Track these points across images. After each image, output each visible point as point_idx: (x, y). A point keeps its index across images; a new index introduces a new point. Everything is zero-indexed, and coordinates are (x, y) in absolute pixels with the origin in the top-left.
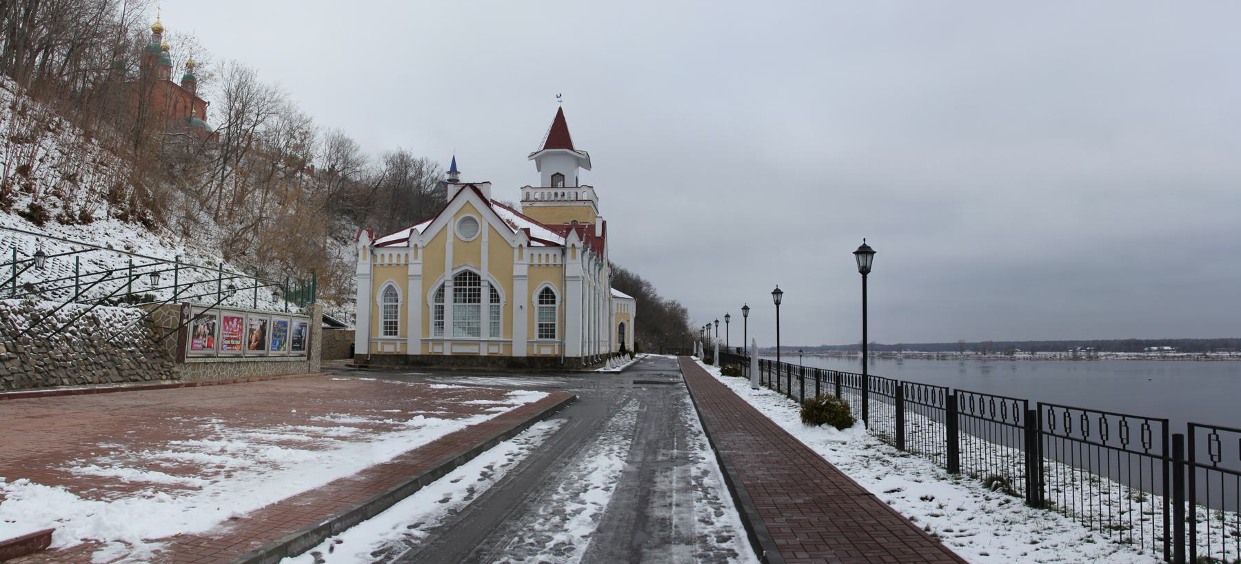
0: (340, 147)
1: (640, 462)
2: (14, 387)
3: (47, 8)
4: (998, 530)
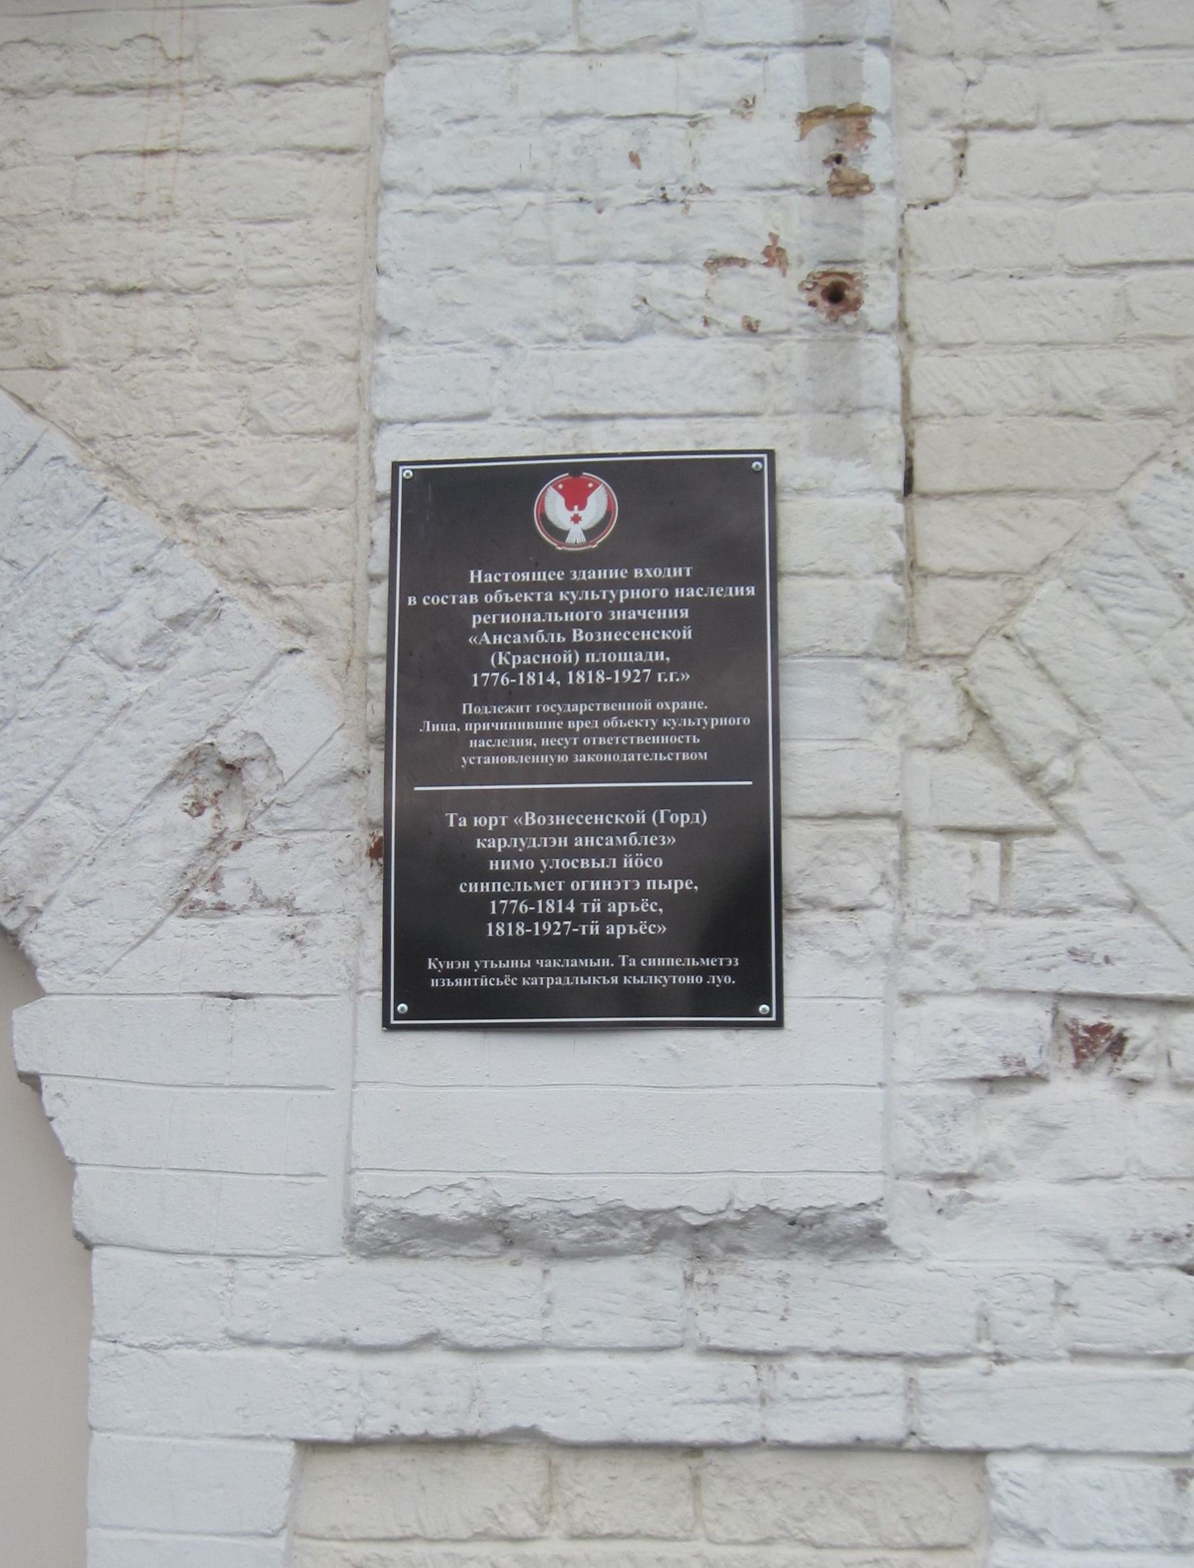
0: (925, 1004)
2: (399, 1008)
4: (838, 1331)
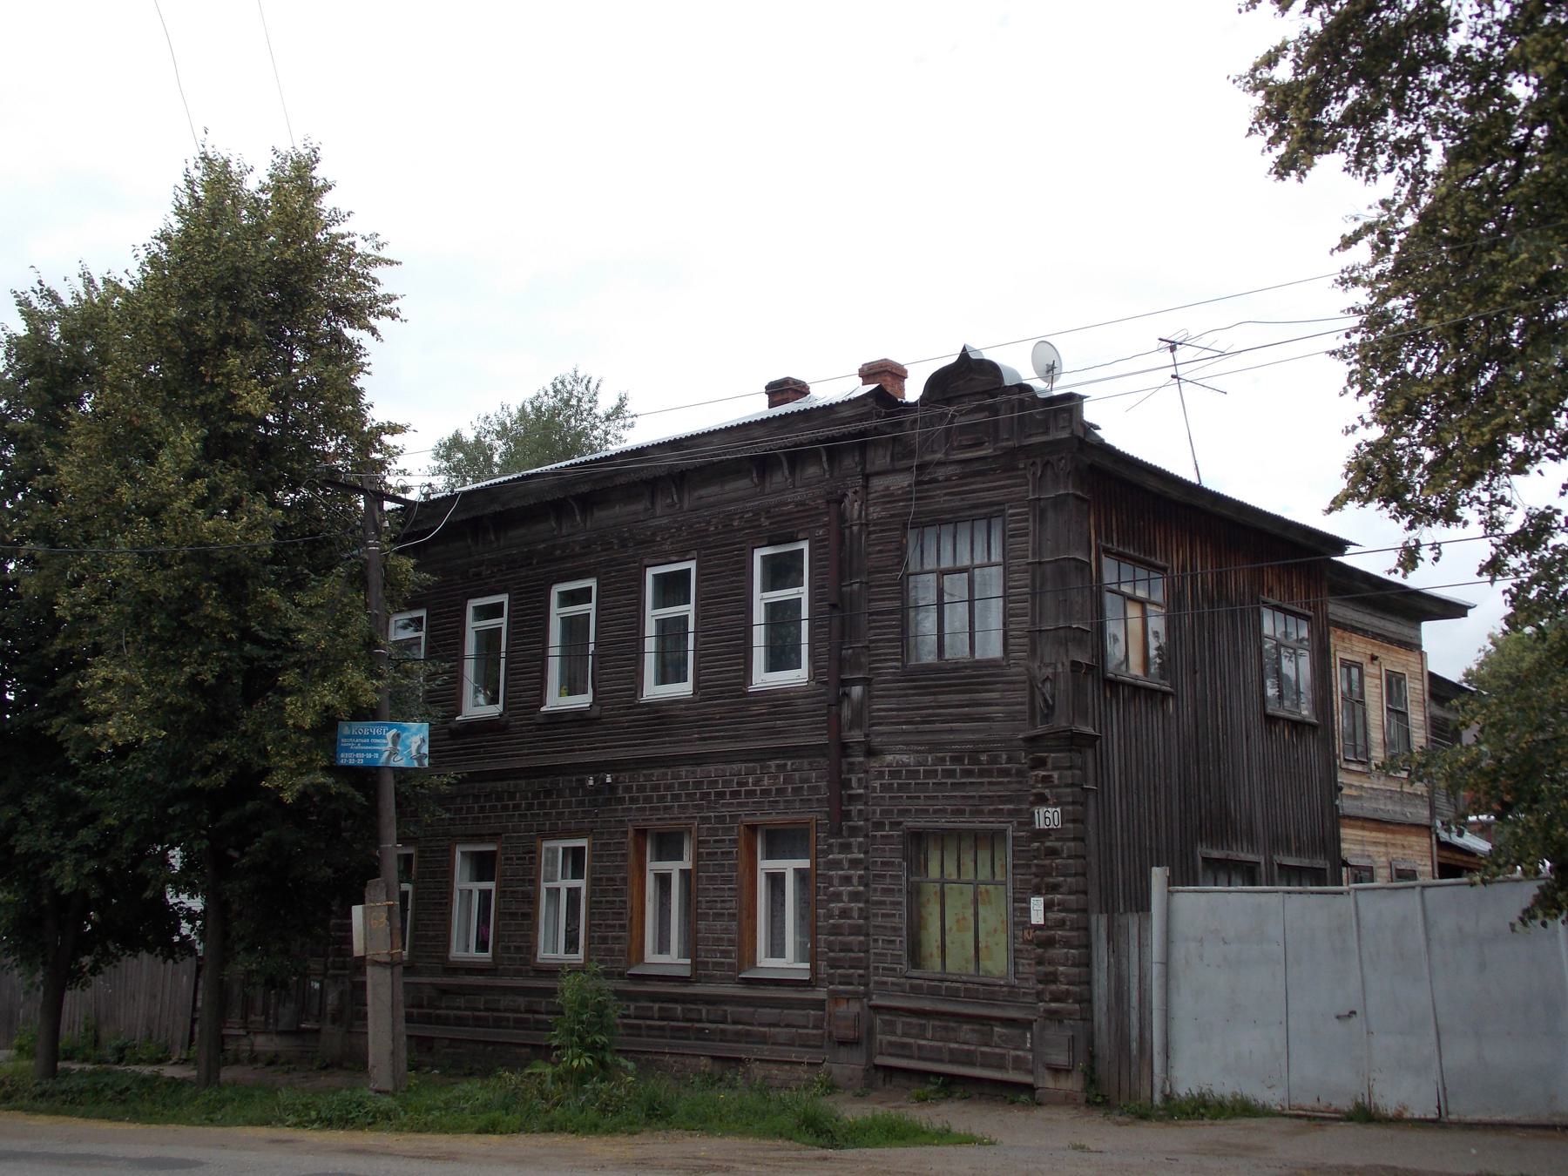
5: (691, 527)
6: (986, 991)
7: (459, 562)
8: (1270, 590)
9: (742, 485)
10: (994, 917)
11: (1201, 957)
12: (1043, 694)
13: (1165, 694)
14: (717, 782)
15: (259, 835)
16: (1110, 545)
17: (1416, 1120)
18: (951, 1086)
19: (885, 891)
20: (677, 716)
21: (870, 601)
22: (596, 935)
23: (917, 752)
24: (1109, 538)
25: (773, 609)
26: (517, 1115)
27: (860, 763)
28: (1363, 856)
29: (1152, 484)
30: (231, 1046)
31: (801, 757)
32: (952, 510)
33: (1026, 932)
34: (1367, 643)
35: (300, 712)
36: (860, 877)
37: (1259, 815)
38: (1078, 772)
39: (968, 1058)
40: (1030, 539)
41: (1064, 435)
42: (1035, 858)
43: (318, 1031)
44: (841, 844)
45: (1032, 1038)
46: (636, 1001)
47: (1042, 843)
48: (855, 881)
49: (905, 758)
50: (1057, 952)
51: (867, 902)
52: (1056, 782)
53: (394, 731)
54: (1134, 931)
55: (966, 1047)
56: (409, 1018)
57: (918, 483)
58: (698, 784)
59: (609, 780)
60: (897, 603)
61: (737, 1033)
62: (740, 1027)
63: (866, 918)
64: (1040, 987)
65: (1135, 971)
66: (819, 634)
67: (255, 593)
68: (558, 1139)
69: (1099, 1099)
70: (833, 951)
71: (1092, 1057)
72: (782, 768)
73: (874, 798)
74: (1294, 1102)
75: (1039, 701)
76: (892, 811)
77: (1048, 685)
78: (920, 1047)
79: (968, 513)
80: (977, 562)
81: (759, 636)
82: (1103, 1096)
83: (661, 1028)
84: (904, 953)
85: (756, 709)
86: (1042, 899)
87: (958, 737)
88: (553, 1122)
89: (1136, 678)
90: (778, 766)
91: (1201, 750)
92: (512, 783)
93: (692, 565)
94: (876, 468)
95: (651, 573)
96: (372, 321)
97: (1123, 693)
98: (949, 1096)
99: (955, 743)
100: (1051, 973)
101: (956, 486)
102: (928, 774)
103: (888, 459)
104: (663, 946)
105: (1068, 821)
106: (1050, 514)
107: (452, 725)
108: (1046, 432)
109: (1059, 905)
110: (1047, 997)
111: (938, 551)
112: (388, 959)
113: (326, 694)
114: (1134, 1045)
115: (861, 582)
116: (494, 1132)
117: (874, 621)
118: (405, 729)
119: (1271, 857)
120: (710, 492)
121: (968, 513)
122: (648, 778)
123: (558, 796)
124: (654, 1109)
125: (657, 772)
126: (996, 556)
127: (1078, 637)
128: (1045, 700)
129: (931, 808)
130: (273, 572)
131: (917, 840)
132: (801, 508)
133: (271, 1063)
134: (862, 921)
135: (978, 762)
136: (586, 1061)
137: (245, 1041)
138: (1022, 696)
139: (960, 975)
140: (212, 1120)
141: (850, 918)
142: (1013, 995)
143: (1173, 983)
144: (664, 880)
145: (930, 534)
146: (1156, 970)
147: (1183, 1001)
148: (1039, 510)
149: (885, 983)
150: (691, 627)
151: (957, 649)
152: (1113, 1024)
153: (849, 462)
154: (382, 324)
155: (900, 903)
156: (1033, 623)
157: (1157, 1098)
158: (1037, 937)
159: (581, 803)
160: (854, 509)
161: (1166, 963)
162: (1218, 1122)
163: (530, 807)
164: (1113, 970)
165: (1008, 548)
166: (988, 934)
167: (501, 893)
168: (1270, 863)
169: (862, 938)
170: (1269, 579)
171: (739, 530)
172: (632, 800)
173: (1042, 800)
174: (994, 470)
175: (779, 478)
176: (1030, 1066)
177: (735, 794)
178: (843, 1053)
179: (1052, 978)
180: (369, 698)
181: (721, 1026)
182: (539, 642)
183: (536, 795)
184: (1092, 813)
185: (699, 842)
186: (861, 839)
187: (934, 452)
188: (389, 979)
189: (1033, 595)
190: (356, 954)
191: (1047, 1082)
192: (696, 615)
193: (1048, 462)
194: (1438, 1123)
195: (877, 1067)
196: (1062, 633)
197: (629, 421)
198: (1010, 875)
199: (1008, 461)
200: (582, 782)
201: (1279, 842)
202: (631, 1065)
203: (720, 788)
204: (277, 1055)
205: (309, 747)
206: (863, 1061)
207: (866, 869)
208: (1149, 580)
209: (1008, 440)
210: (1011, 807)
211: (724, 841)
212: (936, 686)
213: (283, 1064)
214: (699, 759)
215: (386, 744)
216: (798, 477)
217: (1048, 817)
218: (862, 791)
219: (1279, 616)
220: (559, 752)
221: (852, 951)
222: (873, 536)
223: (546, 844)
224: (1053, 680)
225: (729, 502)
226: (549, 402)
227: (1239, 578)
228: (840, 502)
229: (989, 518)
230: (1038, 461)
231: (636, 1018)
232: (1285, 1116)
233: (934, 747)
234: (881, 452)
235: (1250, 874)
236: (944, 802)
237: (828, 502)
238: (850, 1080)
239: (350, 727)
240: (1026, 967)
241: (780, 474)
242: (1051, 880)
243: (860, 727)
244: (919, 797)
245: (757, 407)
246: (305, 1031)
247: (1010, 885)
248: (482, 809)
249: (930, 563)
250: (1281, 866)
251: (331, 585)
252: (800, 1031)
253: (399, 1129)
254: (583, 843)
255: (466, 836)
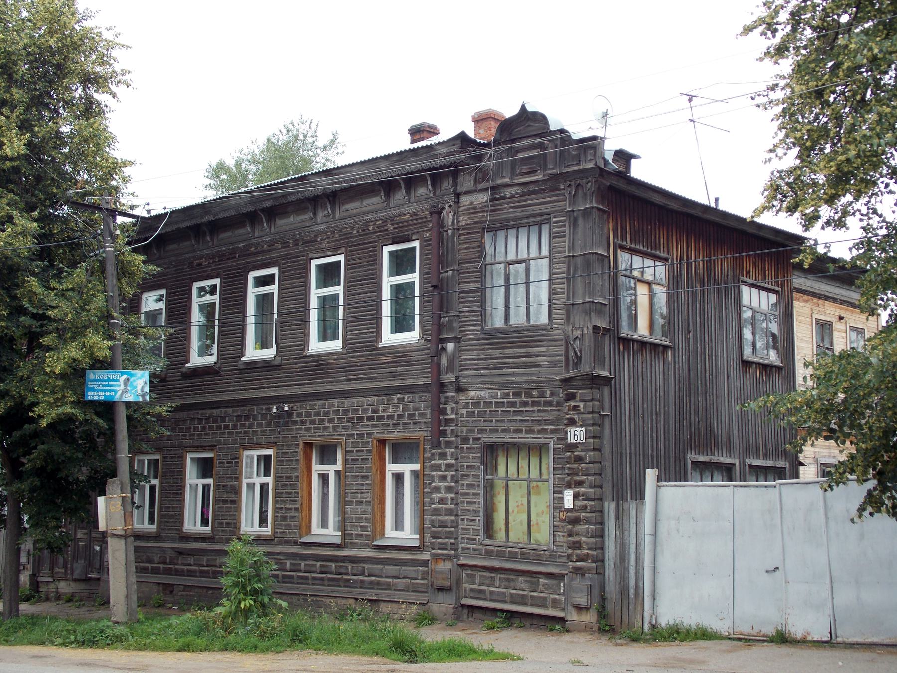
1: (312, 259)
3: (430, 528)
5: (341, 231)
6: (534, 555)
7: (187, 256)
8: (748, 273)
9: (375, 202)
10: (541, 504)
11: (678, 531)
12: (574, 349)
13: (665, 348)
14: (358, 410)
15: (35, 448)
16: (625, 243)
17: (814, 641)
18: (511, 619)
19: (470, 486)
20: (332, 364)
21: (460, 283)
22: (279, 515)
23: (492, 389)
24: (624, 238)
25: (324, 300)
26: (204, 639)
27: (453, 397)
28: (829, 457)
29: (657, 199)
30: (43, 589)
31: (413, 393)
32: (516, 219)
33: (561, 514)
34: (836, 307)
35: (56, 363)
36: (453, 476)
37: (735, 431)
38: (597, 403)
39: (522, 601)
40: (567, 239)
41: (590, 165)
42: (568, 463)
43: (99, 579)
44: (440, 454)
45: (564, 586)
46: (306, 561)
47: (572, 452)
48: (449, 479)
49: (483, 393)
50: (581, 528)
51: (457, 493)
52: (582, 410)
53: (125, 377)
54: (633, 513)
55: (521, 592)
56: (140, 570)
57: (492, 200)
58: (346, 412)
59: (286, 408)
60: (478, 285)
61: (371, 583)
62: (373, 578)
63: (457, 504)
64: (570, 551)
65: (633, 540)
66: (426, 306)
67: (24, 281)
68: (228, 655)
69: (607, 628)
70: (434, 527)
71: (603, 599)
72: (401, 400)
73: (462, 421)
74: (737, 630)
75: (571, 353)
76: (474, 430)
77: (578, 342)
78: (492, 593)
79: (526, 221)
80: (532, 255)
81: (387, 308)
82: (611, 626)
83: (322, 579)
84: (481, 528)
85: (384, 359)
86: (571, 491)
87: (519, 379)
88: (227, 644)
89: (643, 336)
90: (398, 399)
91: (692, 387)
92: (223, 410)
93: (341, 258)
94: (464, 189)
95: (314, 263)
96: (113, 88)
97: (634, 347)
98: (510, 626)
99: (516, 383)
100: (577, 542)
101: (518, 202)
102: (498, 404)
103: (473, 183)
104: (324, 524)
105: (590, 437)
106: (580, 222)
107: (183, 370)
108: (578, 164)
109: (583, 495)
110: (574, 558)
111: (506, 248)
112: (123, 533)
113: (73, 351)
114: (632, 591)
115: (454, 270)
116: (189, 651)
117: (463, 297)
118: (132, 375)
119: (744, 461)
120: (353, 206)
121: (526, 221)
122: (313, 407)
123: (254, 419)
124: (296, 636)
125: (319, 403)
126: (545, 251)
127: (598, 309)
128: (575, 353)
129: (500, 429)
130: (37, 266)
131: (491, 450)
132: (414, 218)
133: (69, 601)
134: (453, 507)
135: (531, 396)
136: (248, 602)
137: (52, 585)
138: (561, 350)
139: (518, 543)
140: (7, 641)
141: (446, 504)
142: (552, 557)
143: (659, 549)
144: (324, 477)
145: (501, 235)
146: (648, 540)
147: (666, 562)
148: (573, 219)
149: (468, 549)
150: (341, 302)
151: (518, 318)
152: (618, 577)
153: (447, 185)
154: (119, 90)
155: (479, 494)
156: (568, 299)
157: (646, 627)
158: (568, 517)
159: (269, 424)
160: (449, 218)
161: (655, 535)
162: (684, 643)
163: (235, 427)
164: (619, 540)
165: (552, 245)
166: (538, 515)
167: (217, 487)
168: (743, 464)
169: (453, 518)
170: (747, 265)
171: (372, 233)
172: (303, 422)
173: (572, 422)
174: (544, 190)
175: (400, 196)
176: (563, 606)
177: (370, 418)
178: (441, 596)
179: (577, 545)
180: (103, 353)
181: (361, 578)
182: (240, 312)
183: (239, 419)
184: (607, 431)
185: (347, 451)
186: (453, 450)
187: (503, 177)
188: (123, 547)
189: (568, 278)
190: (100, 530)
191: (573, 616)
192: (345, 293)
193: (579, 185)
194: (829, 644)
195: (463, 606)
196: (587, 305)
197: (340, 150)
198: (551, 475)
199: (554, 183)
200: (269, 410)
201: (750, 449)
202: (284, 604)
203: (360, 414)
204: (73, 595)
205: (62, 388)
206: (454, 602)
207: (457, 470)
208: (655, 266)
209: (552, 169)
210: (553, 427)
211: (362, 451)
212: (503, 343)
213: (76, 601)
214: (346, 394)
215: (120, 386)
216: (412, 195)
217: (576, 434)
218: (453, 417)
219: (755, 291)
220: (254, 389)
221: (446, 527)
222: (463, 237)
223: (247, 453)
224: (581, 338)
225: (366, 213)
226: (283, 138)
227: (723, 264)
228: (439, 213)
229: (540, 224)
230: (573, 183)
231: (305, 572)
232: (730, 639)
233: (502, 386)
234: (467, 178)
235: (727, 472)
236: (509, 424)
237: (431, 213)
238: (445, 615)
239: (94, 374)
240: (562, 538)
241: (400, 193)
242: (578, 478)
243: (453, 372)
244: (491, 421)
245: (404, 143)
246: (90, 579)
247: (551, 481)
248: (204, 428)
249: (500, 257)
250: (751, 466)
251: (79, 275)
252: (413, 581)
253: (127, 648)
254: (270, 452)
255: (194, 447)
